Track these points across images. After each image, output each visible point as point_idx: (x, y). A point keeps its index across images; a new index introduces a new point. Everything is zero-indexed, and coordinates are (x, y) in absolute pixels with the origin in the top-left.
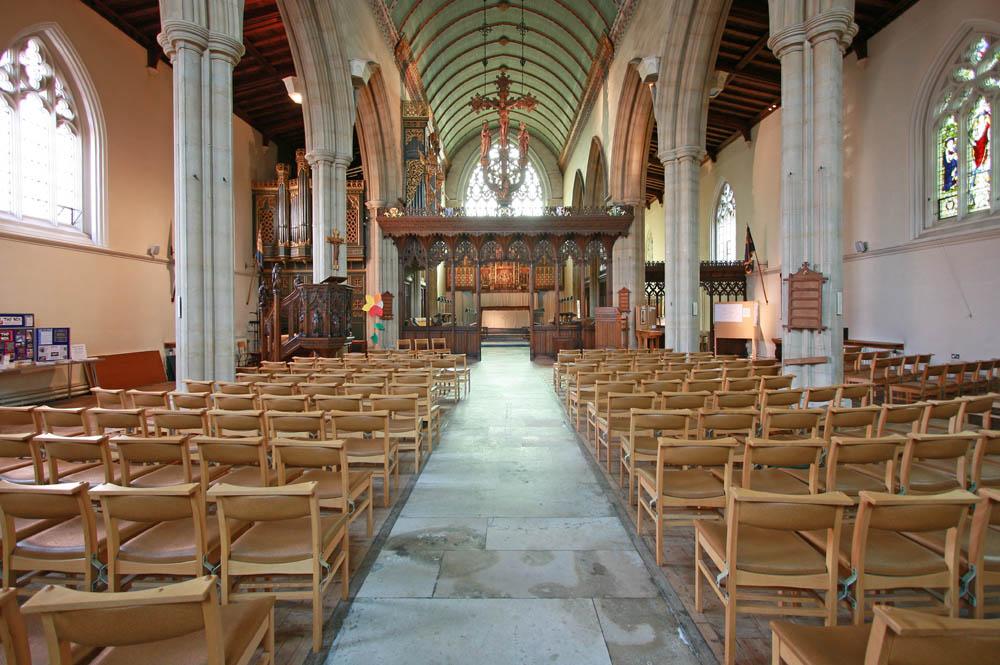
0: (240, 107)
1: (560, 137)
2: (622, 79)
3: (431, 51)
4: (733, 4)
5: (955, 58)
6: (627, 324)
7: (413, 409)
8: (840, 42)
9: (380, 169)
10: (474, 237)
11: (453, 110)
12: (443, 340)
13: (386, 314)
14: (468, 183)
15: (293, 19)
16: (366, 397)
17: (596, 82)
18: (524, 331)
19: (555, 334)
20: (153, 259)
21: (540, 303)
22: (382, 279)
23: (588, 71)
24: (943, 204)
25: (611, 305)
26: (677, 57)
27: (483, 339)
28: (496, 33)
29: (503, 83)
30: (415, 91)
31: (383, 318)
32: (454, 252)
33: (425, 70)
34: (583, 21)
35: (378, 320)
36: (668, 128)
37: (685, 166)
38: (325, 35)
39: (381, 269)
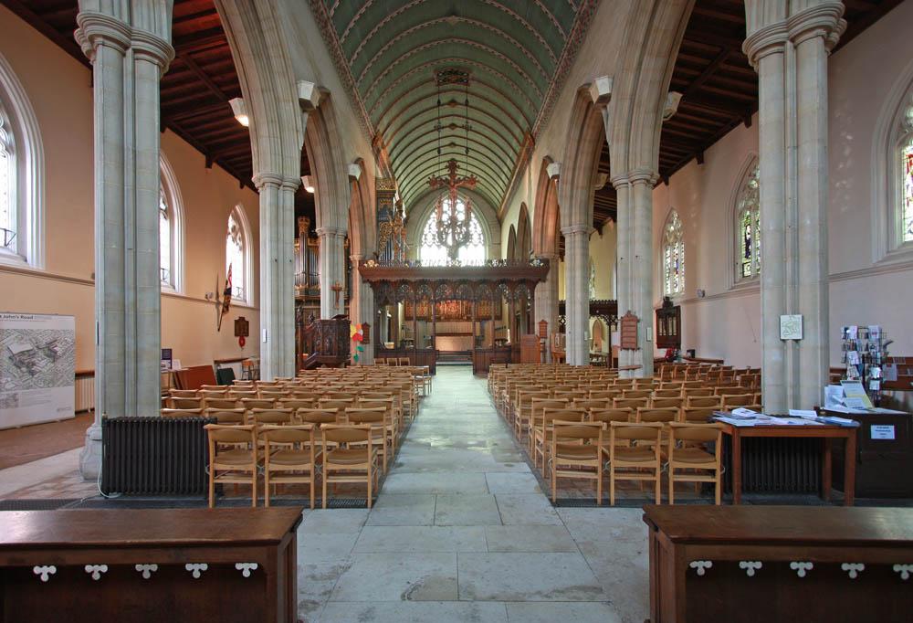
0: (170, 118)
1: (501, 184)
2: (540, 168)
3: (396, 138)
4: (696, 5)
5: (747, 174)
6: (544, 347)
7: (382, 420)
8: (827, 42)
9: (361, 231)
10: (431, 282)
11: (412, 176)
12: (408, 359)
13: (365, 340)
14: (423, 231)
15: (313, 144)
16: (342, 409)
17: (523, 161)
18: (469, 353)
19: (492, 355)
20: (209, 301)
21: (482, 330)
22: (362, 314)
23: (521, 142)
24: (746, 266)
25: (534, 333)
26: (571, 165)
27: (437, 359)
28: (447, 141)
29: (453, 165)
30: (385, 168)
31: (362, 342)
32: (416, 294)
33: (392, 151)
34: (512, 119)
35: (358, 343)
36: (567, 211)
37: (578, 238)
38: (333, 152)
39: (361, 306)
